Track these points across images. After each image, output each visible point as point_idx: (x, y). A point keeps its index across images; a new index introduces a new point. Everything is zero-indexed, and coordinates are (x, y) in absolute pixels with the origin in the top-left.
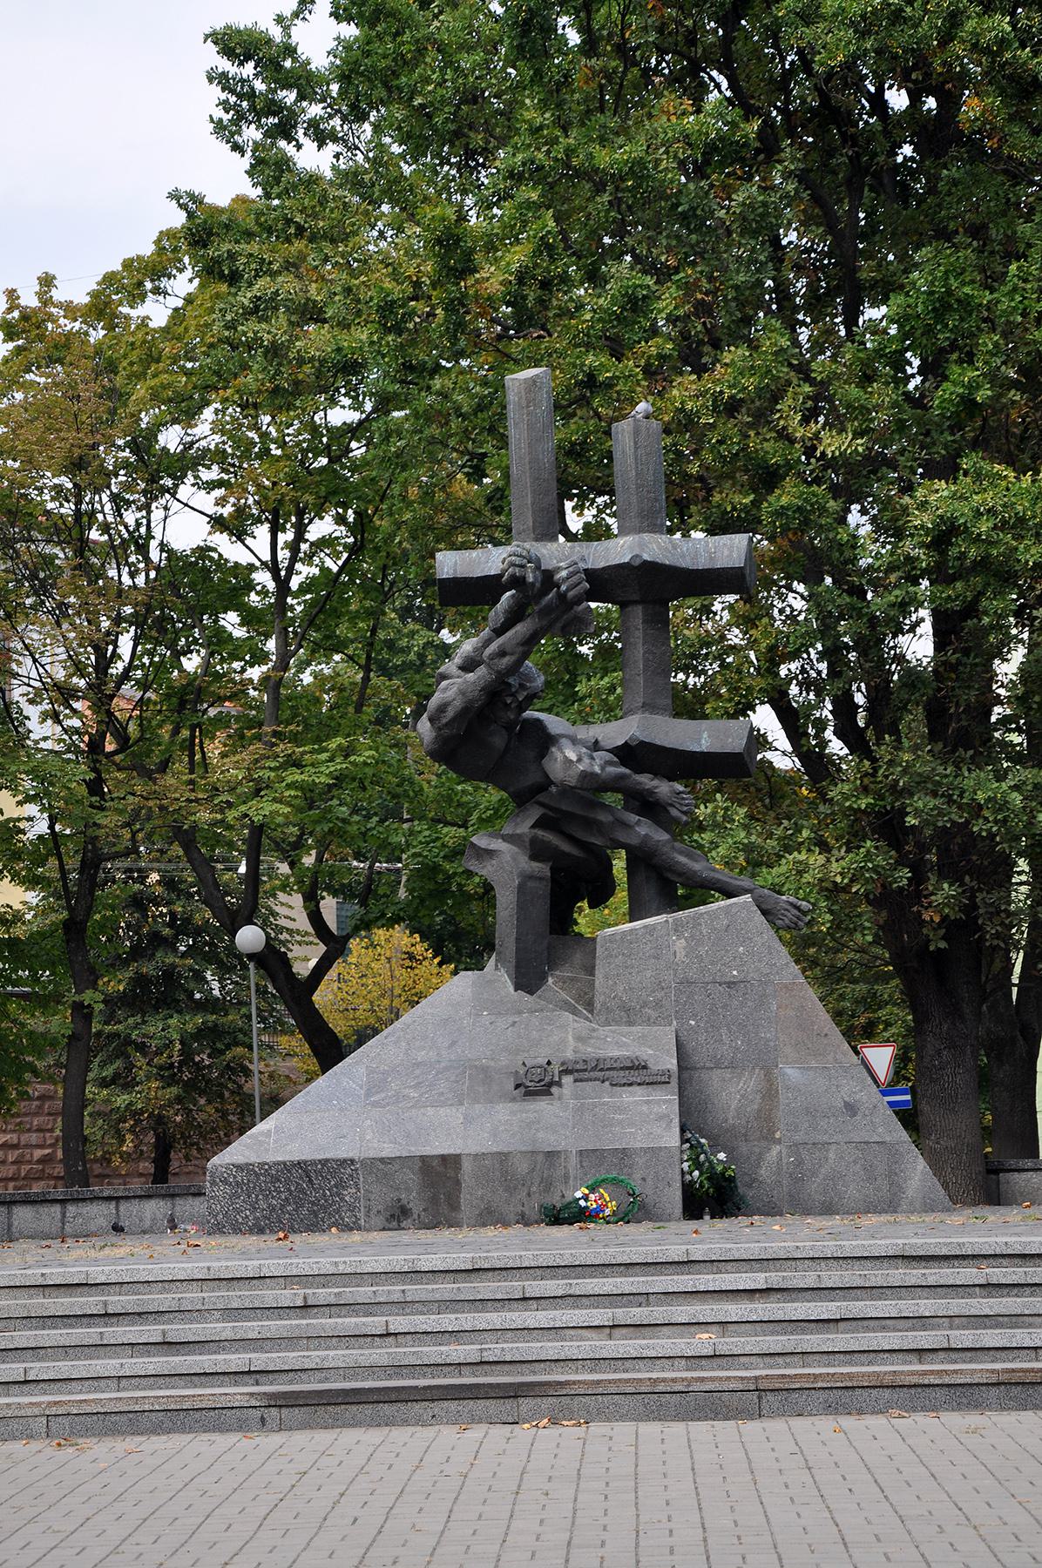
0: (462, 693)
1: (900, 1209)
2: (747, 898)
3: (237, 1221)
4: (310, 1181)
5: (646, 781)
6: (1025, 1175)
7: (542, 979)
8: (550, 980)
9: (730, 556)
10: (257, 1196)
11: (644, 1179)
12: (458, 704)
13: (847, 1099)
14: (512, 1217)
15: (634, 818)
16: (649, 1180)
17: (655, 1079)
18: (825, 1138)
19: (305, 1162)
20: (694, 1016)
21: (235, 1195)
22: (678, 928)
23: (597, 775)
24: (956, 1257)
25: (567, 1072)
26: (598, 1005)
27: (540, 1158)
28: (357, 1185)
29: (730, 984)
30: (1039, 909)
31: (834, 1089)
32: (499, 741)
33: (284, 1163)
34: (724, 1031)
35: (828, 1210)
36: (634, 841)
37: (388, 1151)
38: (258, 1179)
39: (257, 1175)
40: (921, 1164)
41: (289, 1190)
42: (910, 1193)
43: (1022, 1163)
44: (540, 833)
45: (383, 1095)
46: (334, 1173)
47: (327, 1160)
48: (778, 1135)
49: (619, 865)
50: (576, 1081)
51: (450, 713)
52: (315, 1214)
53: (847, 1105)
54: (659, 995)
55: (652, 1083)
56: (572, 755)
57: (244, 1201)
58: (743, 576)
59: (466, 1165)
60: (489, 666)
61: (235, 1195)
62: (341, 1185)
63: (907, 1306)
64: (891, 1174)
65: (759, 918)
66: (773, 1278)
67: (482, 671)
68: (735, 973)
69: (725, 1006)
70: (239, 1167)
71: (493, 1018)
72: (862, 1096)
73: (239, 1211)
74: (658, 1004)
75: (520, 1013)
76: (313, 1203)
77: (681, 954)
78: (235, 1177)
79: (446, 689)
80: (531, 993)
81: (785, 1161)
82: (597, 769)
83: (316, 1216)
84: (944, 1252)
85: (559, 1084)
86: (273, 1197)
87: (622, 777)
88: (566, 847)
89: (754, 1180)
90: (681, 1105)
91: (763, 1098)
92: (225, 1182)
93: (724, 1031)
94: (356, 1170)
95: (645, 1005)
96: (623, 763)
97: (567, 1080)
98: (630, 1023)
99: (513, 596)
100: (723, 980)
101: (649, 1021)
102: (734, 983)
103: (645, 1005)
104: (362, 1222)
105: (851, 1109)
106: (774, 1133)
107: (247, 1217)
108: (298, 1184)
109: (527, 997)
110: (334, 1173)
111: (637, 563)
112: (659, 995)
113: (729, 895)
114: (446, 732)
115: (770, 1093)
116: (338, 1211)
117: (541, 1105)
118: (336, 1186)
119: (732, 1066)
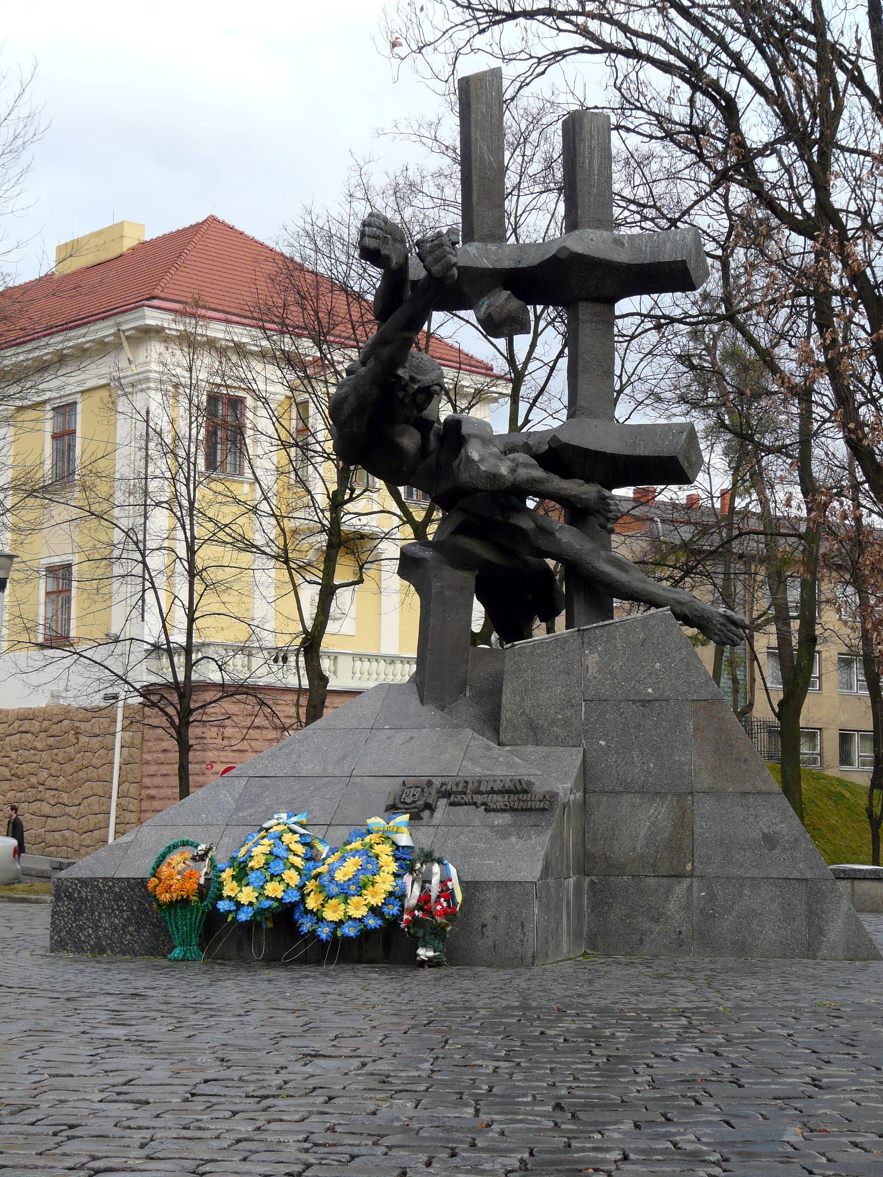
3: (79, 939)
10: (100, 914)
11: (495, 918)
12: (352, 399)
13: (766, 830)
16: (502, 921)
18: (740, 872)
20: (605, 736)
21: (78, 912)
23: (501, 476)
25: (447, 794)
30: (7, 550)
31: (752, 819)
34: (635, 753)
38: (102, 896)
39: (100, 891)
41: (132, 910)
45: (253, 810)
48: (689, 867)
50: (453, 804)
55: (522, 810)
56: (475, 456)
57: (87, 919)
68: (650, 690)
69: (638, 726)
70: (84, 882)
72: (783, 828)
73: (81, 928)
77: (593, 671)
78: (79, 892)
81: (695, 895)
86: (115, 916)
89: (662, 914)
92: (70, 897)
93: (635, 753)
95: (554, 722)
100: (637, 698)
103: (554, 722)
105: (770, 841)
107: (89, 935)
108: (141, 903)
113: (658, 606)
119: (641, 792)
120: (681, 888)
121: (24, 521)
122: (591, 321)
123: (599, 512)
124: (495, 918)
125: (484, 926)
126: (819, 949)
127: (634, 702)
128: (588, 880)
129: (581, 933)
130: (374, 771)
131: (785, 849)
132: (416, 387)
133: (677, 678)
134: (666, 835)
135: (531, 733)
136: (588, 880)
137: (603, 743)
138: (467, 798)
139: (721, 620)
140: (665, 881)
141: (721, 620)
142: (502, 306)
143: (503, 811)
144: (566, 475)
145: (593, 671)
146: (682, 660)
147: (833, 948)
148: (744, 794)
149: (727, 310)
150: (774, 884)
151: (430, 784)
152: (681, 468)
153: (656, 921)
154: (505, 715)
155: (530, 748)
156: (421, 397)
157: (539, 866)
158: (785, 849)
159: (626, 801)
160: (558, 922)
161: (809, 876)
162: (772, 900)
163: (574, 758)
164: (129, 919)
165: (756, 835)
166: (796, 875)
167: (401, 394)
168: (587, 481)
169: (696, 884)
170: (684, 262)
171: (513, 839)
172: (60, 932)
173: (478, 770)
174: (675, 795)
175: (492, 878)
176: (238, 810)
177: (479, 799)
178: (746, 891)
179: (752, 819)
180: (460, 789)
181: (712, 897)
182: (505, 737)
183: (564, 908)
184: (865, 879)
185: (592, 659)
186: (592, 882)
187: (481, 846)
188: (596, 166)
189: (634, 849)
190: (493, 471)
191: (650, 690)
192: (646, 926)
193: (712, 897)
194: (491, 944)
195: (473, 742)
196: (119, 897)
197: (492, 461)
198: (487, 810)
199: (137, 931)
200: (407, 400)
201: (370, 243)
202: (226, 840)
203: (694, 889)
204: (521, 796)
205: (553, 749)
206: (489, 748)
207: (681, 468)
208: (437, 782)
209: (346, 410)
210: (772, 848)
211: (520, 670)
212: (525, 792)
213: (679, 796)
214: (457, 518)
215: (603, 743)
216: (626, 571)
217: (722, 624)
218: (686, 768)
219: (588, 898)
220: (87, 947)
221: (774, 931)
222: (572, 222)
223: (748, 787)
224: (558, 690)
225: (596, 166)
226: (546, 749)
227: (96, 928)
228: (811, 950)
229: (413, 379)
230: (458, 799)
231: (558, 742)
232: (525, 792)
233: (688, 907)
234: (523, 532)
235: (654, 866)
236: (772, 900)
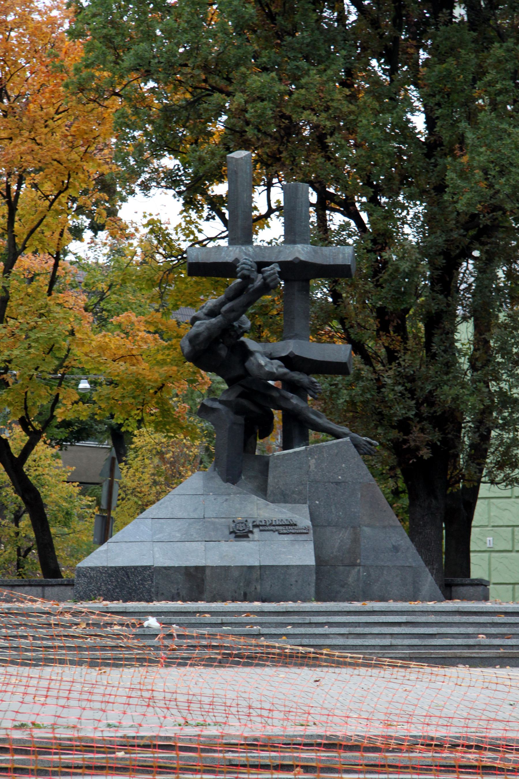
0: (208, 329)
2: (348, 439)
4: (128, 577)
5: (296, 376)
6: (466, 588)
7: (239, 476)
8: (243, 477)
9: (344, 258)
12: (205, 334)
15: (290, 395)
17: (299, 531)
20: (318, 499)
21: (90, 583)
22: (310, 453)
24: (111, 768)
26: (269, 492)
29: (337, 483)
32: (223, 352)
34: (333, 507)
36: (290, 407)
37: (168, 563)
39: (101, 573)
40: (430, 578)
43: (459, 580)
47: (137, 567)
48: (358, 561)
49: (278, 415)
50: (261, 531)
51: (201, 338)
53: (394, 547)
54: (301, 487)
59: (208, 572)
60: (224, 316)
61: (90, 583)
62: (144, 580)
63: (463, 630)
65: (354, 450)
66: (410, 619)
67: (219, 318)
69: (334, 495)
70: (92, 569)
71: (215, 497)
74: (300, 493)
75: (229, 494)
79: (198, 326)
80: (233, 483)
82: (275, 370)
84: (475, 610)
85: (251, 532)
87: (285, 374)
88: (252, 407)
89: (346, 584)
92: (85, 576)
93: (333, 507)
96: (286, 367)
97: (256, 530)
99: (240, 283)
101: (295, 502)
103: (293, 492)
105: (396, 549)
109: (232, 486)
111: (297, 261)
112: (301, 487)
114: (197, 347)
115: (356, 540)
116: (142, 593)
117: (243, 544)
119: (336, 526)
121: (388, 441)
123: (309, 389)
140: (347, 568)
145: (313, 467)
149: (498, 362)
153: (343, 586)
162: (397, 576)
166: (408, 564)
169: (361, 570)
170: (349, 266)
173: (267, 515)
177: (272, 528)
178: (385, 572)
181: (369, 575)
185: (312, 462)
189: (332, 553)
193: (369, 575)
196: (111, 576)
208: (250, 521)
213: (354, 528)
224: (296, 476)
235: (342, 560)
236: (397, 576)
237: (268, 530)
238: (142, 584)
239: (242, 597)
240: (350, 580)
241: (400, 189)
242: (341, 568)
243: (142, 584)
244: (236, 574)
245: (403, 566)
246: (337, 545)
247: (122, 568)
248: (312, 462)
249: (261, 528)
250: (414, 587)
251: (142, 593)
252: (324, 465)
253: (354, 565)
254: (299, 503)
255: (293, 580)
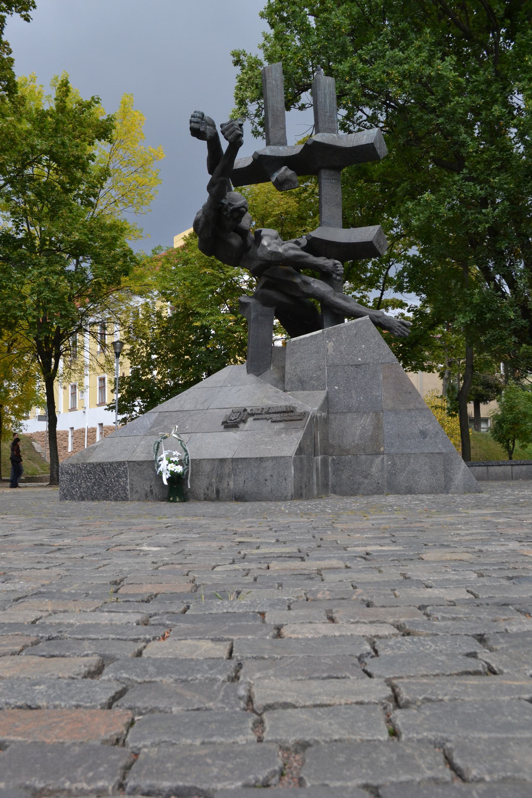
1: (450, 491)
4: (105, 474)
11: (271, 476)
12: (202, 219)
13: (421, 428)
14: (202, 496)
16: (275, 477)
18: (408, 451)
19: (102, 463)
20: (337, 384)
21: (71, 480)
27: (217, 463)
28: (126, 476)
29: (357, 366)
31: (414, 423)
33: (93, 464)
34: (353, 392)
35: (410, 491)
39: (81, 470)
41: (95, 478)
42: (456, 482)
44: (266, 291)
46: (116, 470)
48: (382, 449)
50: (254, 419)
52: (107, 491)
54: (319, 373)
58: (374, 149)
64: (446, 471)
68: (360, 359)
73: (73, 488)
74: (318, 378)
76: (106, 485)
77: (331, 351)
81: (385, 463)
83: (108, 492)
89: (369, 474)
90: (57, 447)
91: (374, 428)
92: (67, 473)
93: (353, 392)
94: (126, 468)
98: (304, 389)
100: (353, 363)
102: (359, 365)
103: (311, 378)
104: (129, 496)
105: (424, 434)
106: (380, 448)
110: (116, 470)
112: (319, 373)
115: (378, 426)
116: (117, 490)
118: (117, 476)
119: (357, 411)
120: (378, 460)
122: (328, 179)
124: (271, 476)
125: (266, 480)
126: (450, 489)
127: (352, 366)
128: (330, 458)
129: (327, 485)
130: (219, 406)
131: (431, 438)
132: (232, 208)
133: (374, 352)
134: (370, 433)
135: (300, 384)
136: (330, 458)
137: (336, 388)
138: (264, 416)
139: (399, 324)
140: (370, 457)
141: (399, 324)
142: (284, 173)
143: (281, 421)
144: (317, 254)
145: (331, 351)
146: (375, 343)
147: (457, 488)
148: (409, 410)
150: (426, 456)
151: (245, 410)
152: (375, 248)
153: (366, 477)
154: (287, 376)
155: (300, 392)
156: (236, 215)
157: (295, 447)
158: (431, 438)
159: (349, 416)
160: (310, 479)
161: (444, 451)
162: (425, 464)
163: (321, 395)
164: (94, 483)
165: (417, 431)
166: (437, 451)
167: (225, 213)
168: (328, 258)
170: (372, 144)
171: (283, 435)
172: (63, 490)
174: (374, 412)
175: (270, 455)
176: (151, 428)
177: (268, 416)
178: (412, 461)
179: (414, 423)
180: (259, 412)
181: (394, 465)
182: (287, 387)
183: (315, 471)
184: (493, 465)
185: (330, 345)
186: (333, 459)
187: (267, 439)
188: (328, 102)
189: (354, 441)
190: (274, 250)
191: (360, 359)
192: (361, 480)
193: (394, 465)
194: (270, 490)
195: (270, 390)
197: (274, 245)
198: (272, 422)
199: (98, 489)
200: (228, 216)
201: (196, 126)
202: (143, 442)
203: (385, 460)
204: (289, 414)
205: (311, 392)
206: (277, 392)
207: (375, 248)
209: (201, 225)
210: (425, 437)
211: (294, 353)
212: (292, 412)
213: (377, 413)
214: (263, 280)
215: (336, 388)
216: (349, 302)
217: (399, 326)
218: (379, 398)
219: (332, 467)
220: (76, 497)
221: (426, 480)
222: (317, 127)
223: (412, 406)
224: (313, 362)
225: (328, 102)
226: (308, 392)
227: (80, 487)
228: (446, 489)
229: (230, 204)
230: (259, 417)
231: (314, 388)
232: (292, 412)
233: (382, 470)
234: (295, 284)
235: (364, 449)
236: (425, 464)
237: (262, 419)
238: (118, 481)
239: (214, 496)
240: (374, 470)
241: (519, 166)
242: (363, 457)
243: (118, 481)
244: (207, 468)
245: (432, 453)
246: (358, 432)
247: (99, 464)
248: (330, 345)
249: (256, 417)
250: (446, 477)
251: (117, 490)
252: (342, 348)
253: (378, 453)
254: (317, 389)
255: (268, 474)
